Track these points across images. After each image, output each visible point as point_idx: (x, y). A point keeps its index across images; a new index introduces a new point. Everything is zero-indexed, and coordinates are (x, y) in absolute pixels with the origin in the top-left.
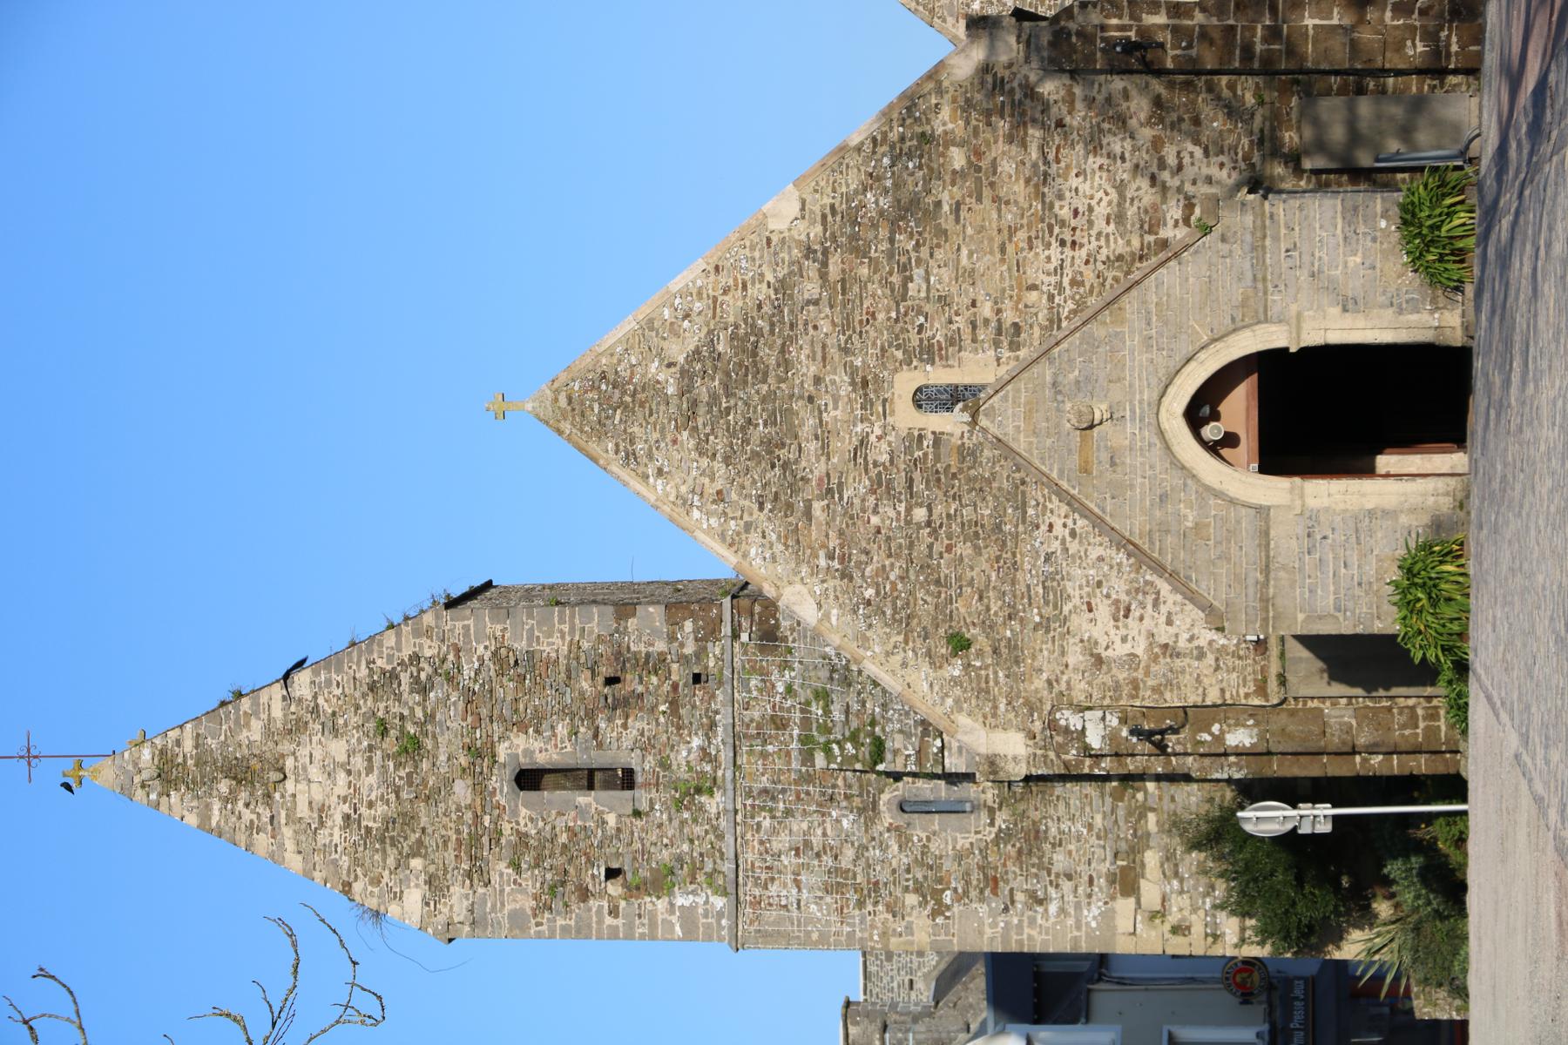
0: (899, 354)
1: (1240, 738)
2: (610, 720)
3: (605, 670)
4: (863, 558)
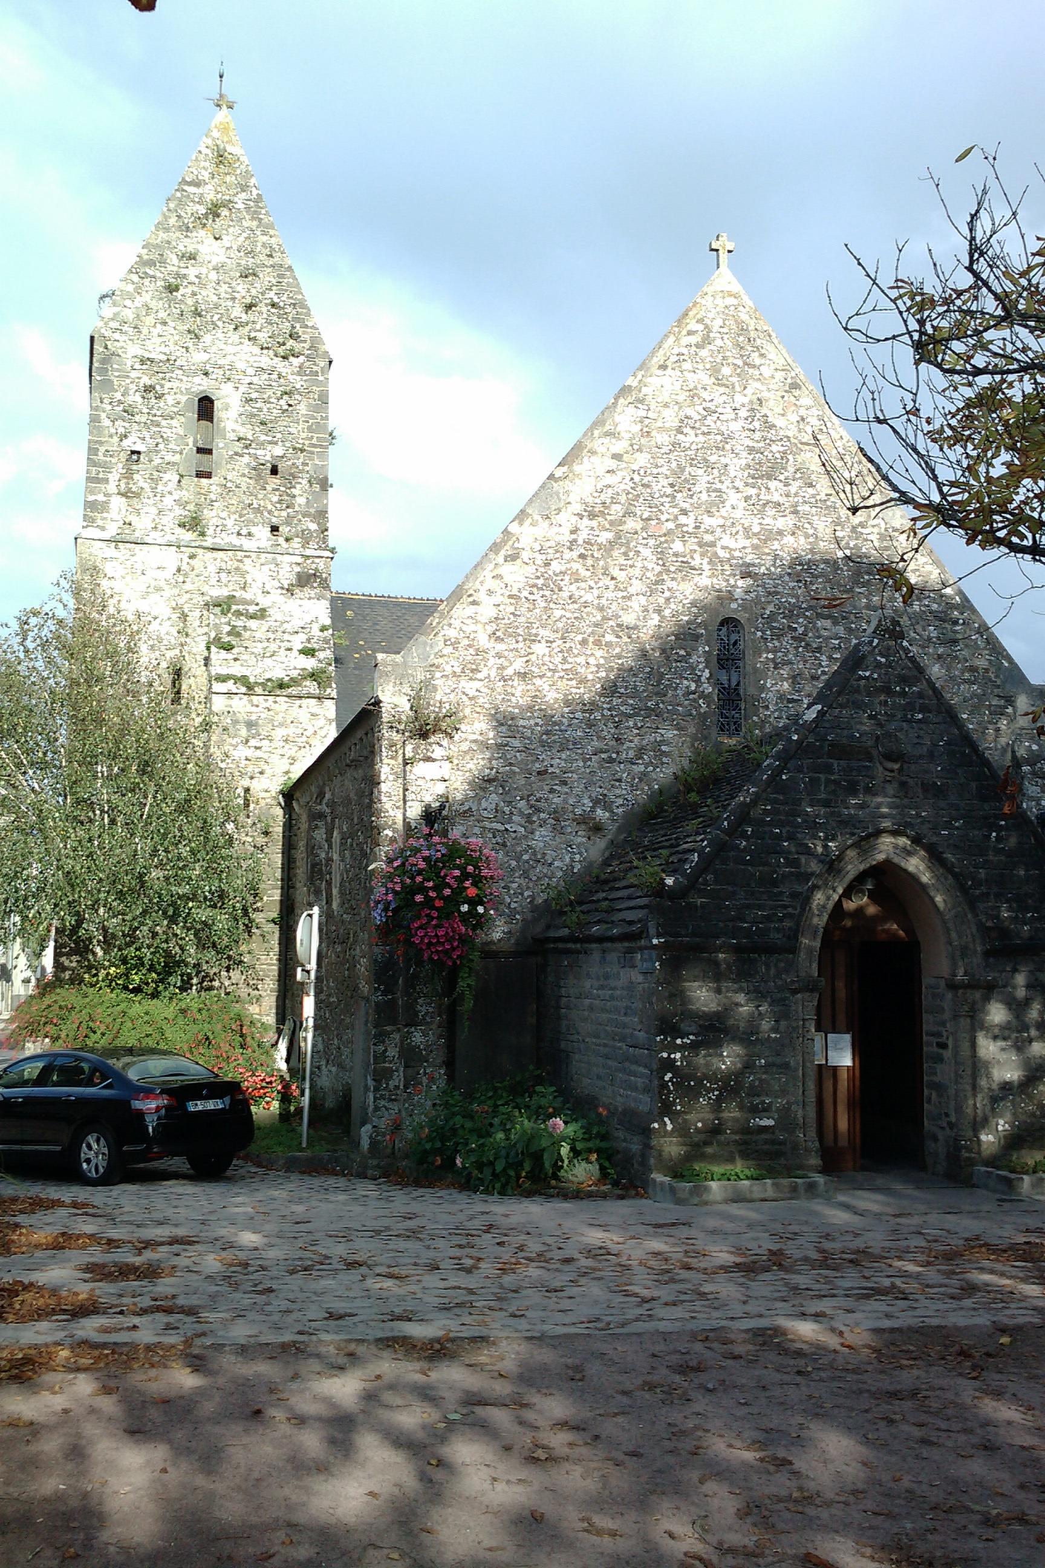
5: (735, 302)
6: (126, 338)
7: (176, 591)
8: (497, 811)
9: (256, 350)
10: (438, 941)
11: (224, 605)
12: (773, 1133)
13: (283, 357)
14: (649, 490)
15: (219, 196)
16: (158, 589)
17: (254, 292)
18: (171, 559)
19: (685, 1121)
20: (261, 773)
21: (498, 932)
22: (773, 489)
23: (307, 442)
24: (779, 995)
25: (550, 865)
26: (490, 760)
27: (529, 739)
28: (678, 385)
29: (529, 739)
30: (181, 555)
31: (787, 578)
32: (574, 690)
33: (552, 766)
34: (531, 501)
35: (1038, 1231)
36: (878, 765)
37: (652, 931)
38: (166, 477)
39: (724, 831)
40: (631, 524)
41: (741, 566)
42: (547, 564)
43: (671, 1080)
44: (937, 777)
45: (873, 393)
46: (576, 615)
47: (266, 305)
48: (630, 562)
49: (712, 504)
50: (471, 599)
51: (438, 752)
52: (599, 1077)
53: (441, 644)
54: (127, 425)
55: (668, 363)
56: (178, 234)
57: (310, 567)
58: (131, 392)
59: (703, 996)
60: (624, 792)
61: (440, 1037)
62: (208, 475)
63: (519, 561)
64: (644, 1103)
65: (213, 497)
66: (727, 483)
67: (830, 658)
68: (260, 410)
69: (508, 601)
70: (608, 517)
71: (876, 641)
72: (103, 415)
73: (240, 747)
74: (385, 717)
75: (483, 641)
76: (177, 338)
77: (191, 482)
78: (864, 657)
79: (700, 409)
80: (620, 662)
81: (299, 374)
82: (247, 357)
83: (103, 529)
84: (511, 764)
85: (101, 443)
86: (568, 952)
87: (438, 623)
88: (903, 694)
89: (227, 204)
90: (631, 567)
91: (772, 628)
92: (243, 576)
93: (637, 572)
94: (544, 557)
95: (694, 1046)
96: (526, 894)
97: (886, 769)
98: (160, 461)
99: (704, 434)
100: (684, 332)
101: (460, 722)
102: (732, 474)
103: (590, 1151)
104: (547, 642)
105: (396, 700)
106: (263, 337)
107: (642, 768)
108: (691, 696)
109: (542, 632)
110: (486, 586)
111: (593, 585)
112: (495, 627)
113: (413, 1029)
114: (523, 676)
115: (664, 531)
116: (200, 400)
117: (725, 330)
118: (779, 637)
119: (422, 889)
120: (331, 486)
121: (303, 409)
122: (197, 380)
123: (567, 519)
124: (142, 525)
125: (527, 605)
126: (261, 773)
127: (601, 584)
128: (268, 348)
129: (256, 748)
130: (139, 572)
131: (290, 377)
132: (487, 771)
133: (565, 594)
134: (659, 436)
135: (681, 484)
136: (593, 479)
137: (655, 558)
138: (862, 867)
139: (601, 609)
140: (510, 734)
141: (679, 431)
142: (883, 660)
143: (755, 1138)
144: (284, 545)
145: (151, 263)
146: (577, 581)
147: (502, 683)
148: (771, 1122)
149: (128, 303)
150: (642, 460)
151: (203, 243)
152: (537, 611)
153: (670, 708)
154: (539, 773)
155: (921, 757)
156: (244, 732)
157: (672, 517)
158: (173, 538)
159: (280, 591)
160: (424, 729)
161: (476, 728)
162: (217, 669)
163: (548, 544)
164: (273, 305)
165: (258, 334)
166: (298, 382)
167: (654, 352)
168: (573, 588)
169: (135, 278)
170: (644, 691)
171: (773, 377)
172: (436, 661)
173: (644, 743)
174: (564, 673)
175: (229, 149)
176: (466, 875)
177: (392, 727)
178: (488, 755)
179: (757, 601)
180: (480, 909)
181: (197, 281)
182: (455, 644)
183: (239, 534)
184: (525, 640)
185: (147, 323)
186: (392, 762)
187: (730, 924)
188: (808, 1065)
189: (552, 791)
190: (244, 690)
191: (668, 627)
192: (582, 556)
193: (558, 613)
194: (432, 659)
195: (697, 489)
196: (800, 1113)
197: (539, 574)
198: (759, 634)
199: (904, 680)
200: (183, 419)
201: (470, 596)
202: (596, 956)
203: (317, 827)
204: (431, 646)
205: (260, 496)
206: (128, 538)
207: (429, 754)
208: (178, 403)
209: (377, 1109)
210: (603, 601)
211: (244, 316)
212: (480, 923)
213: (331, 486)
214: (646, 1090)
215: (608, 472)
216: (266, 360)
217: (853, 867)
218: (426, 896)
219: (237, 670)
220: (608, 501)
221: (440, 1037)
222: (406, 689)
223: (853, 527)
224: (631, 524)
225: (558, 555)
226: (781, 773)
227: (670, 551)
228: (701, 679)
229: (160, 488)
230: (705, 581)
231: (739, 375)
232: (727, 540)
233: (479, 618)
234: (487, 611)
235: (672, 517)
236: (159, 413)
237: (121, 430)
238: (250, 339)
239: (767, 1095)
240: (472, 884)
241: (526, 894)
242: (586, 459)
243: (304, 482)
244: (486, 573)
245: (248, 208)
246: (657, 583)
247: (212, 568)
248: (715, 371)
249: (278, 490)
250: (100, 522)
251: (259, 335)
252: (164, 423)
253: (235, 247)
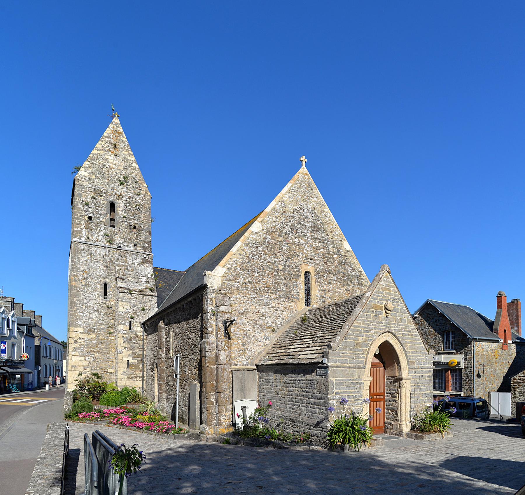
0: (318, 269)
1: (223, 355)
2: (126, 225)
3: (137, 226)
4: (269, 249)
35: (524, 457)
42: (257, 248)
62: (114, 227)
67: (333, 286)
68: (130, 209)
83: (80, 239)
135: (294, 229)
189: (260, 318)
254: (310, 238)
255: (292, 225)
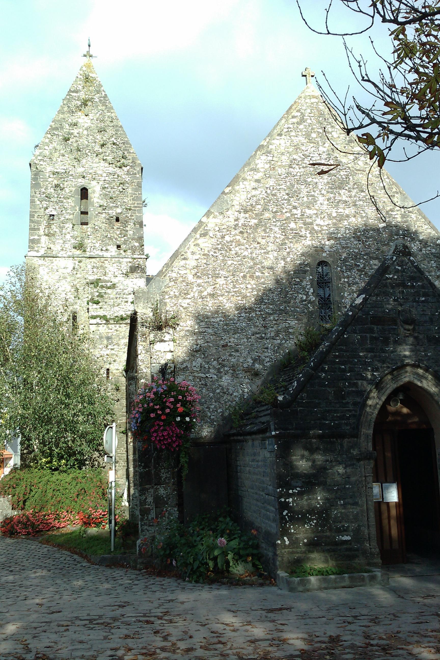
5: (317, 101)
6: (46, 163)
7: (73, 278)
8: (201, 367)
9: (107, 165)
10: (164, 438)
11: (95, 283)
12: (351, 544)
13: (120, 167)
14: (275, 197)
15: (87, 96)
16: (65, 278)
17: (104, 138)
18: (70, 263)
19: (297, 539)
20: (114, 361)
21: (206, 432)
22: (342, 194)
23: (132, 206)
24: (349, 463)
25: (231, 395)
26: (196, 340)
27: (217, 328)
28: (288, 144)
29: (217, 328)
30: (74, 261)
31: (352, 239)
32: (240, 302)
33: (230, 342)
34: (213, 206)
36: (401, 327)
37: (272, 427)
38: (67, 225)
39: (312, 368)
40: (267, 215)
41: (328, 234)
42: (223, 237)
43: (287, 514)
44: (436, 333)
45: (359, 62)
46: (239, 263)
47: (111, 144)
48: (267, 235)
49: (310, 203)
50: (183, 257)
51: (167, 337)
52: (255, 512)
53: (168, 281)
54: (47, 203)
55: (283, 133)
56: (68, 115)
57: (136, 263)
58: (49, 188)
59: (302, 464)
60: (270, 354)
61: (174, 490)
62: (86, 224)
63: (207, 236)
64: (273, 528)
65: (89, 233)
66: (317, 192)
68: (110, 192)
69: (202, 257)
70: (255, 212)
71: (395, 258)
72: (36, 199)
73: (104, 349)
74: (139, 320)
75: (190, 278)
76: (69, 162)
77: (78, 227)
78: (388, 267)
79: (300, 155)
80: (264, 286)
81: (127, 174)
82: (103, 168)
83: (38, 251)
84: (208, 342)
85: (36, 212)
86: (240, 441)
87: (166, 270)
88: (413, 287)
89: (91, 100)
90: (268, 237)
91: (346, 266)
92: (104, 269)
93: (272, 239)
94: (221, 234)
95: (300, 494)
96: (219, 411)
97: (405, 329)
98: (63, 218)
99: (303, 167)
100: (290, 117)
101: (178, 320)
102: (320, 187)
103: (248, 555)
104: (224, 277)
105: (144, 311)
106: (109, 158)
107: (279, 341)
108: (304, 303)
109: (221, 272)
110: (191, 250)
111: (248, 247)
112: (196, 271)
113: (159, 487)
114: (212, 295)
115: (285, 218)
116: (82, 190)
117: (312, 115)
118: (350, 270)
119: (154, 411)
120: (145, 225)
121: (130, 191)
122: (80, 180)
123: (232, 214)
124: (56, 248)
125: (213, 259)
126: (114, 361)
127: (252, 246)
128: (112, 164)
129: (112, 349)
130: (55, 270)
131: (123, 176)
132: (195, 346)
133: (233, 252)
134: (279, 170)
135: (293, 193)
136: (245, 193)
137: (280, 232)
138: (395, 386)
139: (253, 259)
140: (207, 326)
141: (290, 166)
142: (400, 268)
143: (339, 548)
144: (124, 254)
145: (57, 129)
146: (239, 245)
147: (201, 300)
148: (349, 538)
149: (46, 147)
150: (271, 182)
151: (83, 120)
152: (219, 261)
153: (293, 309)
154: (223, 346)
155: (426, 322)
156: (105, 342)
157: (288, 210)
158: (71, 254)
159: (122, 275)
160: (159, 326)
161: (187, 324)
162: (92, 313)
163: (223, 227)
164: (114, 144)
165: (107, 157)
166: (127, 178)
167: (275, 128)
168: (237, 249)
169: (49, 136)
170: (278, 301)
171: (339, 137)
172: (165, 290)
173: (280, 328)
174: (235, 292)
175: (91, 75)
176: (177, 401)
177: (143, 325)
178: (195, 337)
179: (337, 252)
180: (188, 419)
181: (78, 135)
182: (175, 280)
183: (102, 250)
184: (212, 277)
185: (56, 156)
186: (144, 344)
187: (318, 422)
188: (370, 503)
189: (231, 355)
190: (104, 322)
191: (290, 267)
192: (241, 232)
193: (230, 262)
194: (163, 289)
195: (301, 195)
196: (366, 532)
197: (219, 243)
198: (339, 269)
199: (412, 279)
200: (74, 199)
201: (182, 255)
202: (250, 443)
203: (131, 384)
204: (163, 282)
205: (111, 232)
206: (49, 255)
207: (163, 338)
208: (71, 191)
209: (142, 531)
210: (254, 255)
211: (100, 150)
212: (189, 427)
213: (145, 225)
214: (274, 521)
215: (253, 189)
216: (111, 169)
217: (390, 386)
218: (157, 414)
219: (101, 313)
220: (254, 203)
221: (174, 490)
222: (150, 305)
223: (387, 212)
224: (267, 215)
225: (228, 232)
226: (343, 334)
227: (289, 228)
228: (309, 293)
229: (64, 231)
230: (308, 242)
231: (321, 137)
232: (319, 221)
233: (187, 266)
234: (192, 263)
235: (288, 210)
236: (62, 197)
237: (45, 206)
238: (103, 160)
239: (346, 522)
240: (181, 405)
241: (219, 411)
242: (241, 183)
243: (132, 224)
244: (190, 243)
245: (100, 101)
246: (282, 244)
247: (89, 267)
248: (308, 135)
249: (119, 228)
250: (36, 249)
251: (108, 158)
252: (65, 201)
253: (95, 119)
254: (326, 202)
255: (288, 188)
